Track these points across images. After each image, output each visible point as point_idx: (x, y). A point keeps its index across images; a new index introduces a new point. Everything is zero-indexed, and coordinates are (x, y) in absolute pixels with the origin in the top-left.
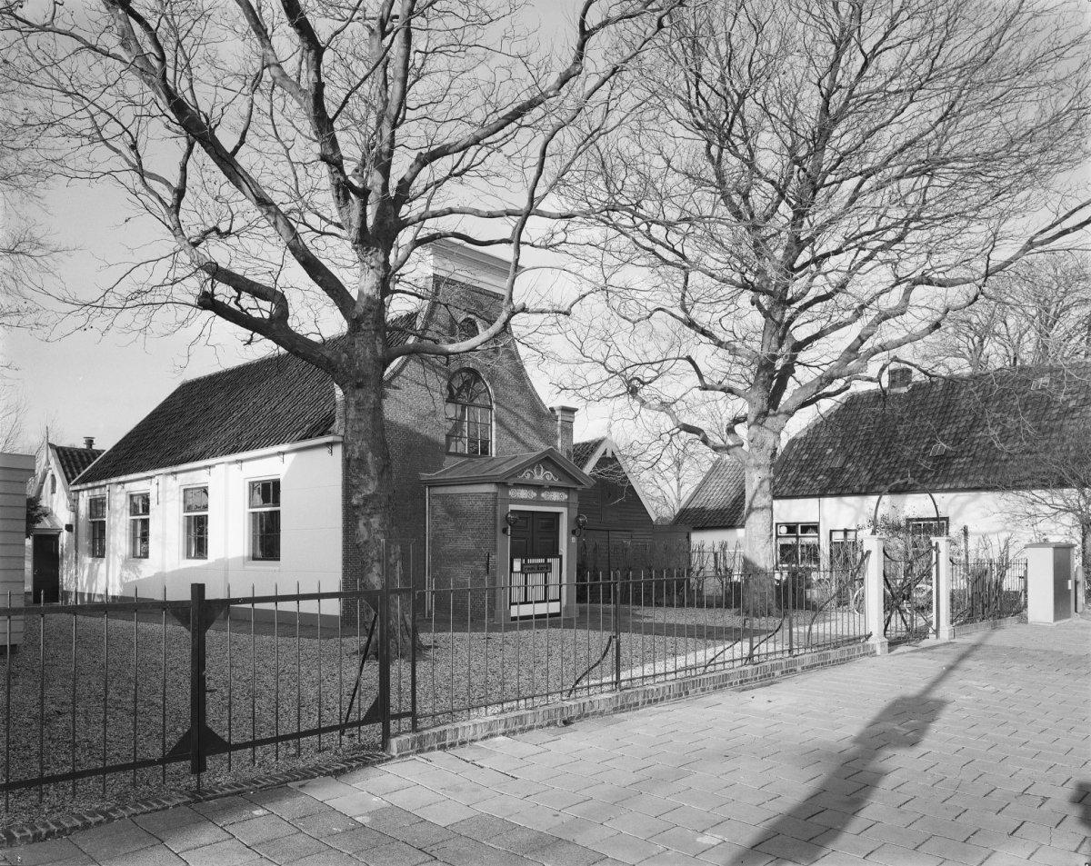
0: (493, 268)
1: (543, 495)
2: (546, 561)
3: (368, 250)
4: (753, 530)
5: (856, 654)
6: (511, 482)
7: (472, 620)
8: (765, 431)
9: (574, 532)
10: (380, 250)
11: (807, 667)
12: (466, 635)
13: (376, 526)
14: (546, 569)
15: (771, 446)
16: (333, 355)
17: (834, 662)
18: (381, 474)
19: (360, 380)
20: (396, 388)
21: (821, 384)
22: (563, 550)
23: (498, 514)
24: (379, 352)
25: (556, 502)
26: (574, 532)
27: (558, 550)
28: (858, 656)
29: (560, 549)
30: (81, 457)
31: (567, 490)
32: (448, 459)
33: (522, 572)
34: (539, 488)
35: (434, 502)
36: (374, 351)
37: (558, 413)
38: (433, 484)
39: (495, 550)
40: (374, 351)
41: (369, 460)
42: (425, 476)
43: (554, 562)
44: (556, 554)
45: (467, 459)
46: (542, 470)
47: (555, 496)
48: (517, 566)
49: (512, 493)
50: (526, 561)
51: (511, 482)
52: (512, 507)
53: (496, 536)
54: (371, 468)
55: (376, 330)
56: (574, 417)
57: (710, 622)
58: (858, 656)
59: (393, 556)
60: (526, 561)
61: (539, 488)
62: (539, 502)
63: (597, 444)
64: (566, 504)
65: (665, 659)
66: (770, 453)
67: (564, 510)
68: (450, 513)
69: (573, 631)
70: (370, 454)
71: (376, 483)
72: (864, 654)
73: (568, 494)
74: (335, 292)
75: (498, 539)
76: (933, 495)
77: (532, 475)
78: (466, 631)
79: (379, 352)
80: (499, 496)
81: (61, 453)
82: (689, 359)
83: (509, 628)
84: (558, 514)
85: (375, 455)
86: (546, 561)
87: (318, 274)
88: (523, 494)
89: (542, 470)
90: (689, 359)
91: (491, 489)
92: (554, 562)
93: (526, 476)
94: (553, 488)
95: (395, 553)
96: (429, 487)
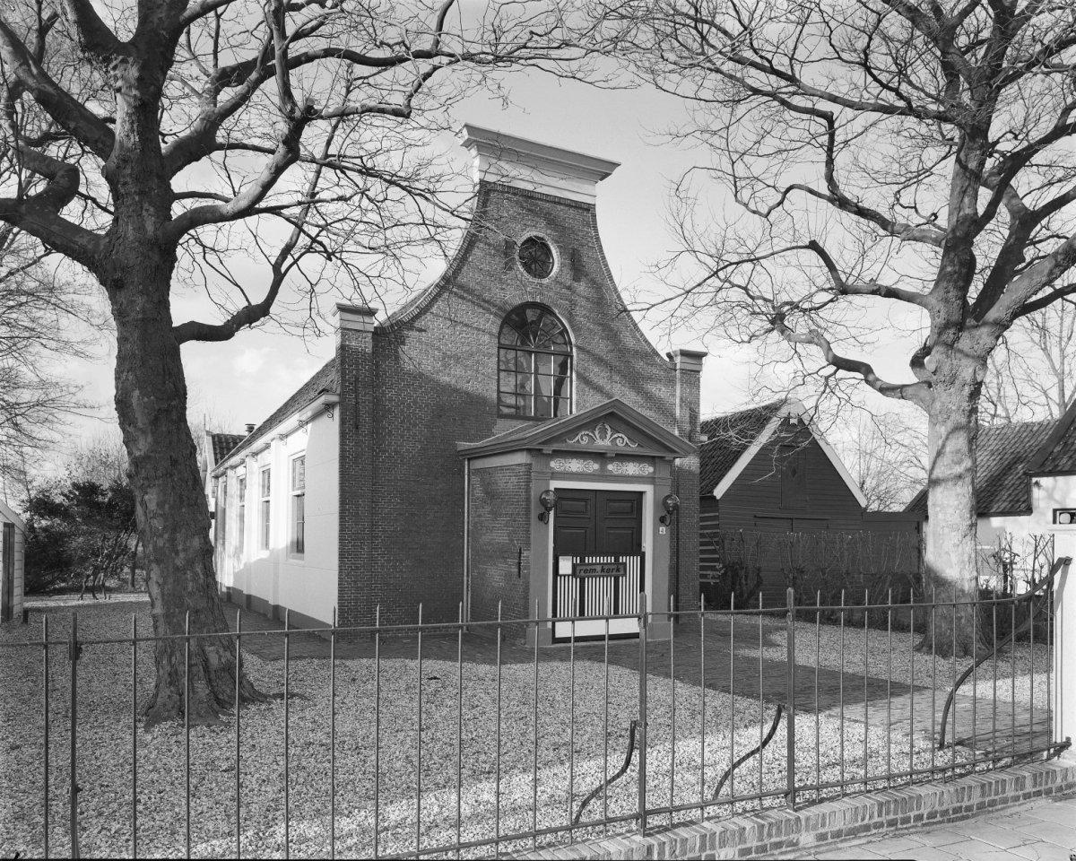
0: (570, 167)
1: (610, 467)
2: (617, 560)
3: (107, 60)
4: (940, 516)
5: (1010, 793)
6: (548, 449)
7: (503, 639)
8: (958, 355)
9: (662, 520)
10: (131, 60)
11: (838, 834)
12: (414, 664)
13: (152, 506)
14: (617, 572)
15: (968, 379)
16: (89, 242)
17: (932, 815)
18: (155, 422)
19: (118, 275)
20: (420, 330)
21: (1057, 265)
22: (647, 545)
23: (532, 493)
24: (150, 227)
25: (632, 477)
26: (662, 520)
27: (640, 545)
28: (1016, 799)
29: (643, 544)
30: (228, 443)
31: (651, 460)
32: (501, 423)
33: (574, 574)
34: (600, 456)
35: (475, 479)
36: (141, 228)
37: (678, 360)
38: (474, 455)
39: (528, 544)
40: (141, 228)
41: (134, 401)
42: (464, 445)
43: (632, 562)
44: (636, 550)
45: (531, 423)
46: (609, 433)
47: (631, 469)
48: (566, 566)
49: (555, 464)
50: (582, 560)
51: (548, 449)
52: (555, 484)
53: (529, 524)
54: (138, 415)
55: (141, 193)
56: (701, 365)
57: (832, 660)
58: (1016, 799)
59: (182, 555)
60: (582, 560)
61: (600, 456)
62: (603, 476)
63: (773, 409)
64: (651, 480)
65: (703, 733)
66: (967, 390)
67: (648, 489)
68: (487, 493)
69: (604, 666)
70: (137, 393)
71: (150, 439)
72: (1038, 794)
73: (654, 465)
74: (100, 146)
75: (532, 528)
76: (934, 283)
77: (592, 440)
78: (453, 659)
79: (150, 227)
80: (534, 468)
81: (216, 439)
82: (813, 246)
83: (546, 656)
84: (641, 494)
85: (143, 394)
86: (617, 560)
87: (67, 118)
88: (575, 465)
89: (609, 433)
90: (813, 246)
91: (521, 458)
92: (632, 562)
93: (582, 440)
94: (623, 457)
95: (184, 550)
96: (469, 460)
